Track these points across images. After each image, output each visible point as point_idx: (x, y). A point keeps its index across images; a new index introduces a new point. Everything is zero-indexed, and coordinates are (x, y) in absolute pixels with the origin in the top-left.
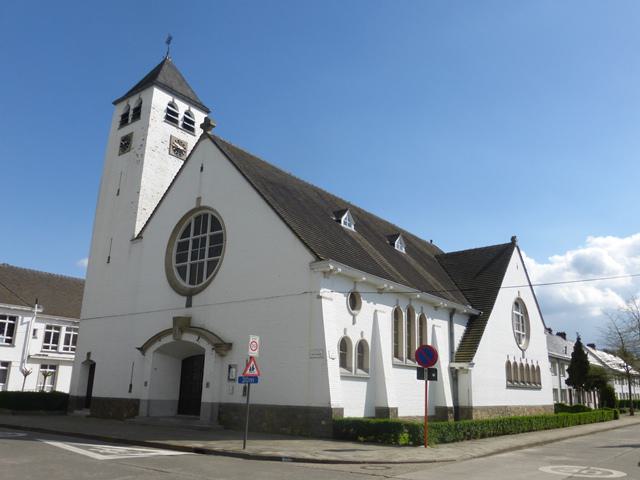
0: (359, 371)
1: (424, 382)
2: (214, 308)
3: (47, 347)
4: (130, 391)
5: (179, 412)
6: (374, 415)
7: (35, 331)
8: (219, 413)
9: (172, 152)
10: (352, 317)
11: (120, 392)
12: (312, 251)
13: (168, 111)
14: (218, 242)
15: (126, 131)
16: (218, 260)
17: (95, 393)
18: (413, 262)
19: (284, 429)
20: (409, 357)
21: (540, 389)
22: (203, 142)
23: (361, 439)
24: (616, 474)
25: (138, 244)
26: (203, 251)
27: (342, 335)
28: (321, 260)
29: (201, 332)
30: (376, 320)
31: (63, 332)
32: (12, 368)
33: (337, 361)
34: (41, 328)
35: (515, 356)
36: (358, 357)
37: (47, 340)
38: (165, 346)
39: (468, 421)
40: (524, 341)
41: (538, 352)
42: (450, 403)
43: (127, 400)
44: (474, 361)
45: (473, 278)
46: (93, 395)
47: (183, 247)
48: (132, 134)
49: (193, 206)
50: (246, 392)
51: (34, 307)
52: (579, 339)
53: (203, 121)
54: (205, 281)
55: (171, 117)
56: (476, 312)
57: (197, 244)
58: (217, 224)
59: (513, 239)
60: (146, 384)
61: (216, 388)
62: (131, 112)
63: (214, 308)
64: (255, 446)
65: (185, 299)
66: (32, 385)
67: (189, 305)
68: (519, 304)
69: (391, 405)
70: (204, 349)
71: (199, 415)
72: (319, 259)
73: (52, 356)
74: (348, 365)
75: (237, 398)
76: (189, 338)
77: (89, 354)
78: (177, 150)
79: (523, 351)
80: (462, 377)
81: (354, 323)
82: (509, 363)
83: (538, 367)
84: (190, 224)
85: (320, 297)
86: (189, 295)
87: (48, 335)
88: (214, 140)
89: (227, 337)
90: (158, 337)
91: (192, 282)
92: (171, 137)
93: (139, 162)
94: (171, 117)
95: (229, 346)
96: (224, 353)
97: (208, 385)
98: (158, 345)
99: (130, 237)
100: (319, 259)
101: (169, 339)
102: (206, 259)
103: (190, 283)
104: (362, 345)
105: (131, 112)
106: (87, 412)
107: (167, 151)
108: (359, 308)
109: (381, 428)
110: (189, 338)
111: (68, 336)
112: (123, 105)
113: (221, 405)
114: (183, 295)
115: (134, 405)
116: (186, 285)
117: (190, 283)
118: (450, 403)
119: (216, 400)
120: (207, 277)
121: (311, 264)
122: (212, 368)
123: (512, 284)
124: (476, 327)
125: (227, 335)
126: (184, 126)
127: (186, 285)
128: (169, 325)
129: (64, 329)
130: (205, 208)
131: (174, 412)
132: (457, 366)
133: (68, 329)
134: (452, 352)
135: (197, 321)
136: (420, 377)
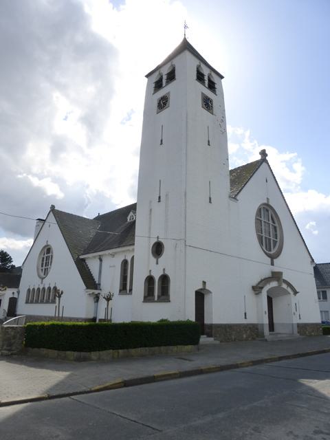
4: (246, 318)
10: (269, 259)
15: (161, 93)
20: (125, 288)
27: (148, 274)
48: (169, 93)
62: (165, 77)
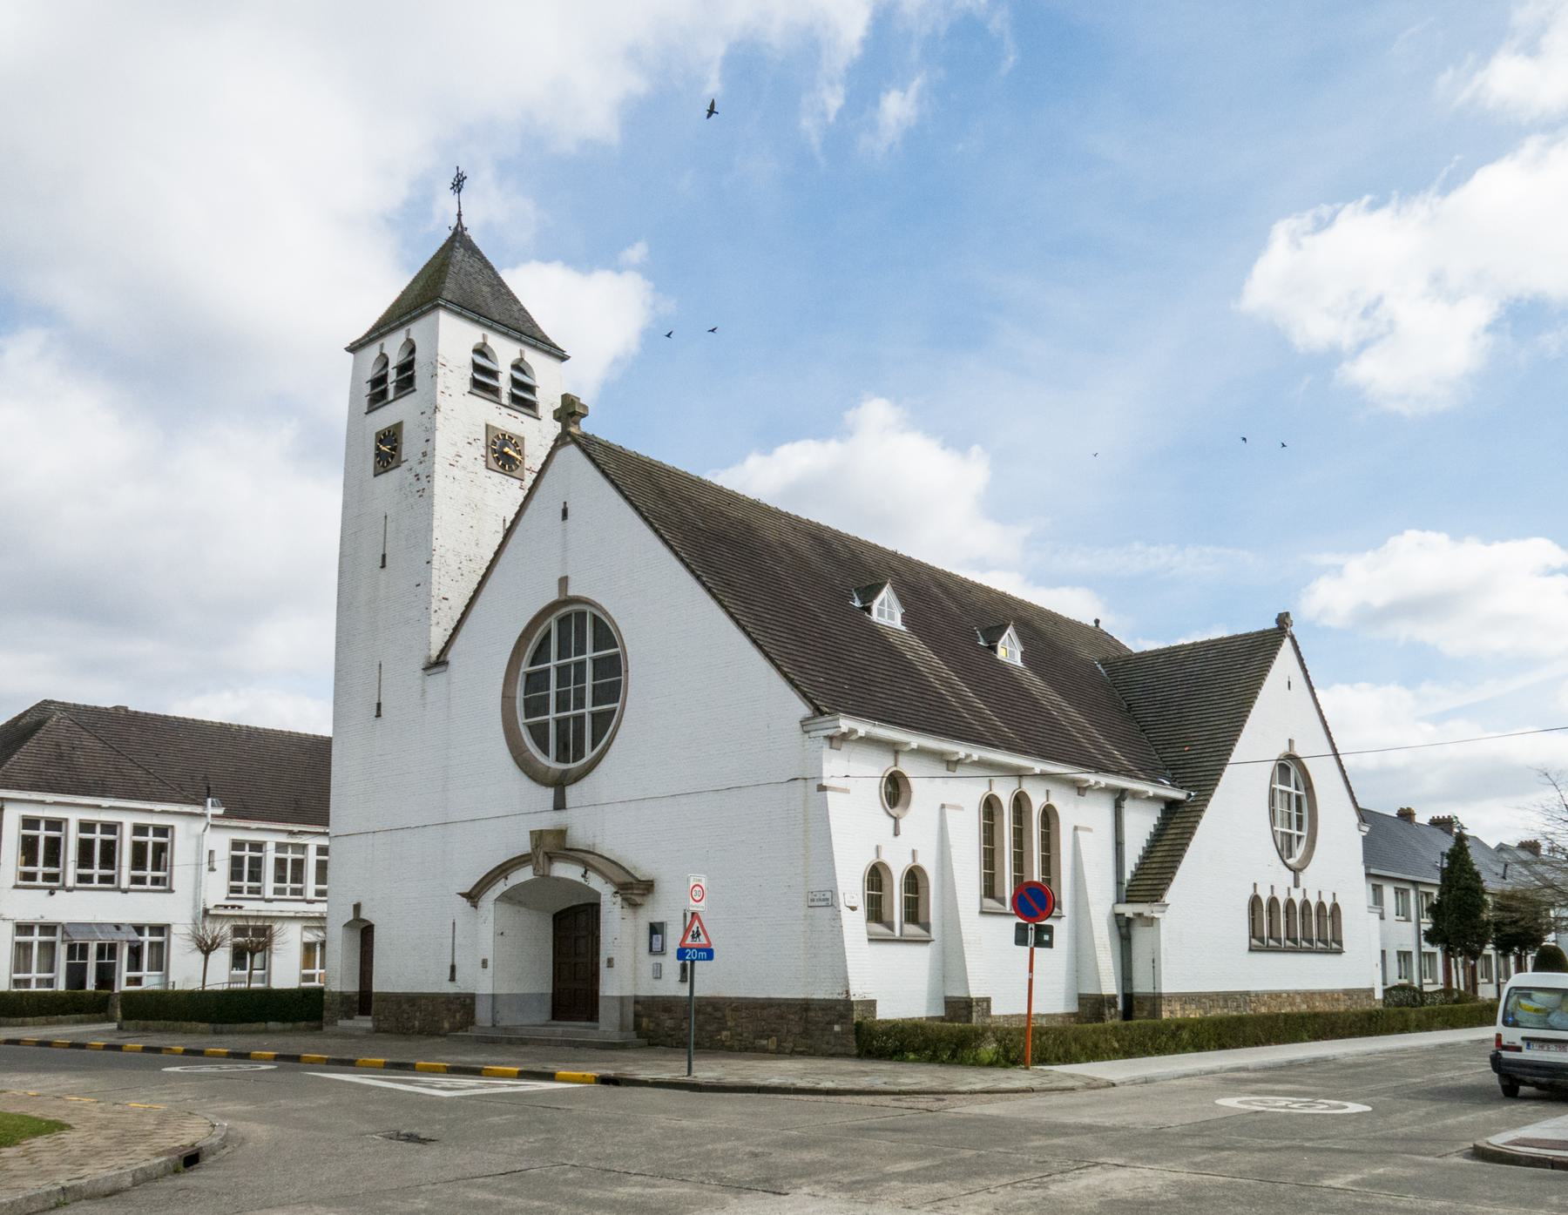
0: (912, 930)
1: (1027, 949)
2: (618, 810)
3: (238, 890)
4: (452, 979)
5: (553, 1018)
6: (942, 1013)
7: (211, 852)
8: (637, 1015)
9: (493, 465)
11: (434, 982)
12: (804, 695)
13: (477, 368)
14: (611, 671)
15: (385, 417)
16: (614, 711)
17: (377, 987)
18: (1036, 684)
19: (764, 1042)
21: (1339, 952)
22: (562, 453)
23: (912, 1056)
24: (1354, 1108)
25: (438, 680)
26: (580, 693)
27: (871, 859)
28: (822, 714)
29: (585, 858)
30: (946, 813)
31: (270, 857)
32: (173, 938)
33: (862, 913)
34: (220, 843)
35: (1275, 881)
36: (901, 902)
37: (236, 874)
38: (514, 888)
39: (1100, 1025)
40: (1299, 852)
41: (1337, 869)
42: (1110, 986)
43: (447, 995)
44: (1167, 898)
45: (1165, 716)
46: (375, 989)
47: (536, 682)
48: (399, 426)
49: (553, 595)
50: (686, 975)
51: (204, 804)
52: (69, 1127)
53: (558, 404)
54: (589, 755)
55: (483, 381)
56: (1179, 795)
57: (568, 685)
58: (605, 634)
59: (1283, 620)
60: (484, 964)
61: (628, 969)
62: (392, 375)
63: (618, 810)
64: (708, 1070)
65: (551, 792)
66: (220, 974)
67: (560, 804)
68: (1289, 766)
69: (975, 993)
70: (598, 895)
71: (597, 1020)
72: (818, 712)
73: (251, 907)
74: (886, 918)
75: (671, 986)
76: (566, 871)
77: (357, 908)
78: (503, 454)
79: (1296, 871)
80: (1140, 935)
81: (896, 834)
82: (1255, 902)
83: (1336, 907)
84: (549, 632)
85: (822, 788)
86: (560, 785)
87: (236, 862)
88: (591, 448)
89: (644, 870)
90: (503, 870)
91: (562, 756)
92: (487, 426)
93: (424, 479)
94: (483, 381)
95: (648, 887)
96: (638, 900)
97: (610, 962)
98: (501, 887)
99: (422, 663)
100: (818, 712)
101: (525, 875)
102: (589, 708)
103: (558, 760)
104: (914, 878)
105: (392, 375)
106: (366, 1023)
107: (481, 462)
108: (907, 804)
109: (955, 1035)
110: (566, 871)
111: (280, 863)
112: (373, 352)
113: (637, 1000)
114: (547, 785)
115: (464, 1005)
116: (550, 762)
117: (558, 760)
118: (1416, 985)
119: (628, 991)
120: (594, 747)
121: (804, 722)
122: (619, 930)
123: (1273, 721)
124: (1176, 825)
125: (642, 863)
126: (515, 399)
127: (550, 762)
128: (524, 846)
129: (312, 851)
130: (577, 600)
131: (545, 1015)
132: (1129, 910)
133: (280, 847)
134: (1119, 883)
135: (580, 835)
136: (1021, 939)
